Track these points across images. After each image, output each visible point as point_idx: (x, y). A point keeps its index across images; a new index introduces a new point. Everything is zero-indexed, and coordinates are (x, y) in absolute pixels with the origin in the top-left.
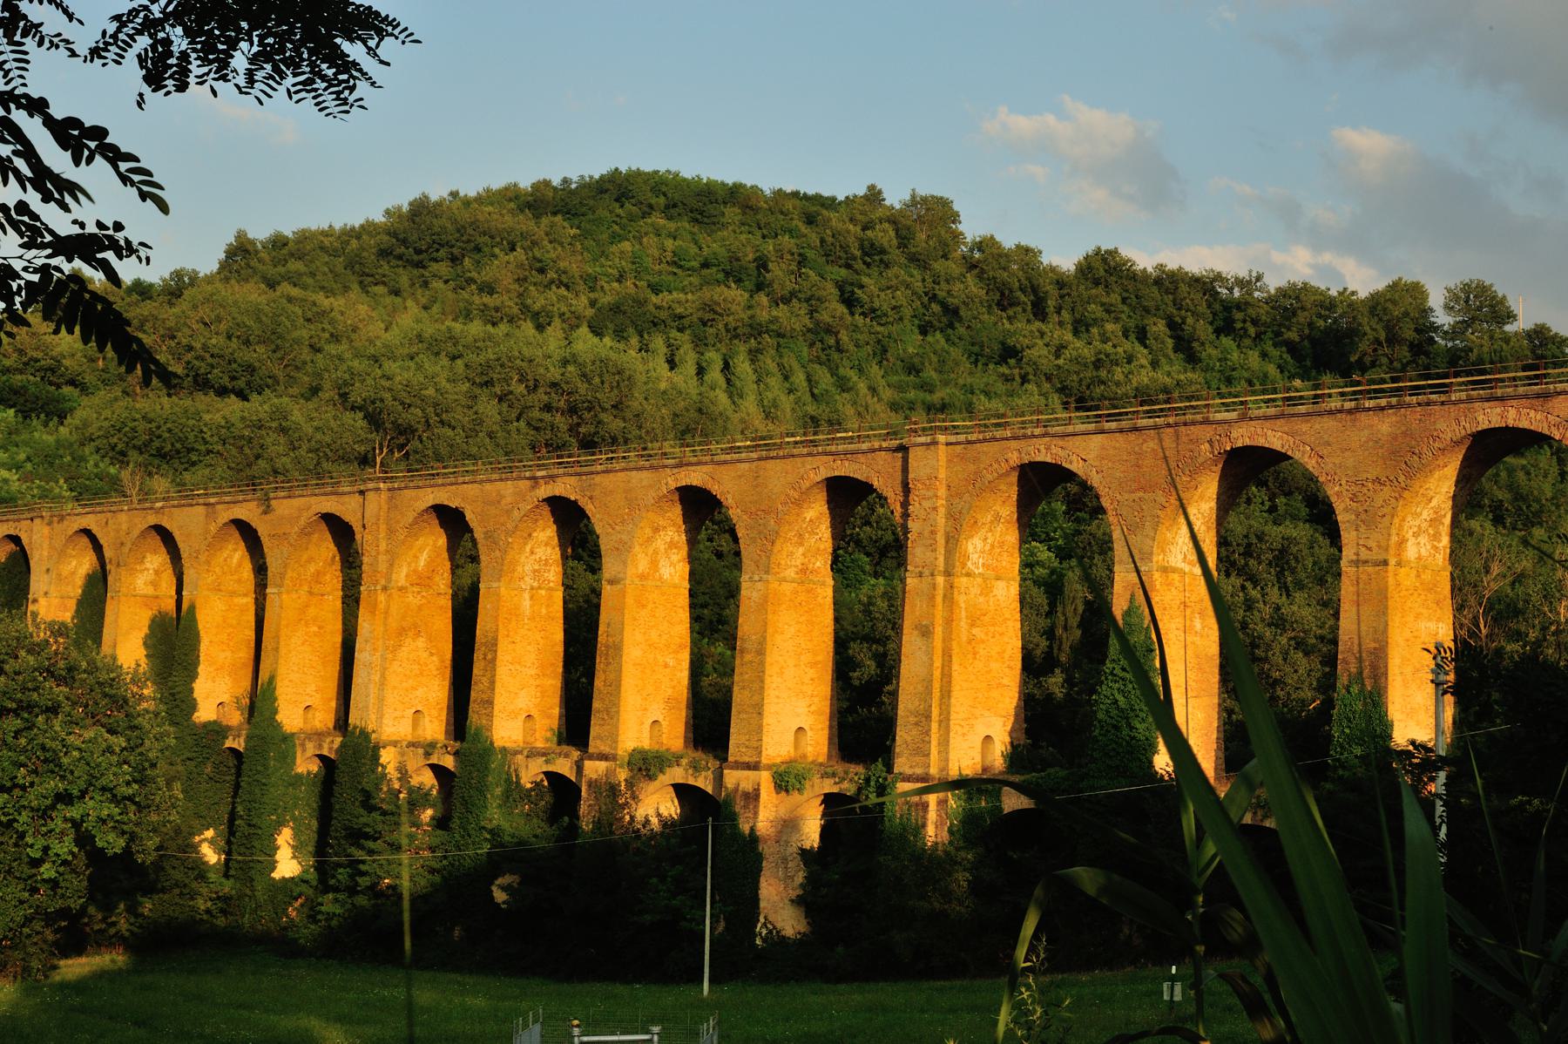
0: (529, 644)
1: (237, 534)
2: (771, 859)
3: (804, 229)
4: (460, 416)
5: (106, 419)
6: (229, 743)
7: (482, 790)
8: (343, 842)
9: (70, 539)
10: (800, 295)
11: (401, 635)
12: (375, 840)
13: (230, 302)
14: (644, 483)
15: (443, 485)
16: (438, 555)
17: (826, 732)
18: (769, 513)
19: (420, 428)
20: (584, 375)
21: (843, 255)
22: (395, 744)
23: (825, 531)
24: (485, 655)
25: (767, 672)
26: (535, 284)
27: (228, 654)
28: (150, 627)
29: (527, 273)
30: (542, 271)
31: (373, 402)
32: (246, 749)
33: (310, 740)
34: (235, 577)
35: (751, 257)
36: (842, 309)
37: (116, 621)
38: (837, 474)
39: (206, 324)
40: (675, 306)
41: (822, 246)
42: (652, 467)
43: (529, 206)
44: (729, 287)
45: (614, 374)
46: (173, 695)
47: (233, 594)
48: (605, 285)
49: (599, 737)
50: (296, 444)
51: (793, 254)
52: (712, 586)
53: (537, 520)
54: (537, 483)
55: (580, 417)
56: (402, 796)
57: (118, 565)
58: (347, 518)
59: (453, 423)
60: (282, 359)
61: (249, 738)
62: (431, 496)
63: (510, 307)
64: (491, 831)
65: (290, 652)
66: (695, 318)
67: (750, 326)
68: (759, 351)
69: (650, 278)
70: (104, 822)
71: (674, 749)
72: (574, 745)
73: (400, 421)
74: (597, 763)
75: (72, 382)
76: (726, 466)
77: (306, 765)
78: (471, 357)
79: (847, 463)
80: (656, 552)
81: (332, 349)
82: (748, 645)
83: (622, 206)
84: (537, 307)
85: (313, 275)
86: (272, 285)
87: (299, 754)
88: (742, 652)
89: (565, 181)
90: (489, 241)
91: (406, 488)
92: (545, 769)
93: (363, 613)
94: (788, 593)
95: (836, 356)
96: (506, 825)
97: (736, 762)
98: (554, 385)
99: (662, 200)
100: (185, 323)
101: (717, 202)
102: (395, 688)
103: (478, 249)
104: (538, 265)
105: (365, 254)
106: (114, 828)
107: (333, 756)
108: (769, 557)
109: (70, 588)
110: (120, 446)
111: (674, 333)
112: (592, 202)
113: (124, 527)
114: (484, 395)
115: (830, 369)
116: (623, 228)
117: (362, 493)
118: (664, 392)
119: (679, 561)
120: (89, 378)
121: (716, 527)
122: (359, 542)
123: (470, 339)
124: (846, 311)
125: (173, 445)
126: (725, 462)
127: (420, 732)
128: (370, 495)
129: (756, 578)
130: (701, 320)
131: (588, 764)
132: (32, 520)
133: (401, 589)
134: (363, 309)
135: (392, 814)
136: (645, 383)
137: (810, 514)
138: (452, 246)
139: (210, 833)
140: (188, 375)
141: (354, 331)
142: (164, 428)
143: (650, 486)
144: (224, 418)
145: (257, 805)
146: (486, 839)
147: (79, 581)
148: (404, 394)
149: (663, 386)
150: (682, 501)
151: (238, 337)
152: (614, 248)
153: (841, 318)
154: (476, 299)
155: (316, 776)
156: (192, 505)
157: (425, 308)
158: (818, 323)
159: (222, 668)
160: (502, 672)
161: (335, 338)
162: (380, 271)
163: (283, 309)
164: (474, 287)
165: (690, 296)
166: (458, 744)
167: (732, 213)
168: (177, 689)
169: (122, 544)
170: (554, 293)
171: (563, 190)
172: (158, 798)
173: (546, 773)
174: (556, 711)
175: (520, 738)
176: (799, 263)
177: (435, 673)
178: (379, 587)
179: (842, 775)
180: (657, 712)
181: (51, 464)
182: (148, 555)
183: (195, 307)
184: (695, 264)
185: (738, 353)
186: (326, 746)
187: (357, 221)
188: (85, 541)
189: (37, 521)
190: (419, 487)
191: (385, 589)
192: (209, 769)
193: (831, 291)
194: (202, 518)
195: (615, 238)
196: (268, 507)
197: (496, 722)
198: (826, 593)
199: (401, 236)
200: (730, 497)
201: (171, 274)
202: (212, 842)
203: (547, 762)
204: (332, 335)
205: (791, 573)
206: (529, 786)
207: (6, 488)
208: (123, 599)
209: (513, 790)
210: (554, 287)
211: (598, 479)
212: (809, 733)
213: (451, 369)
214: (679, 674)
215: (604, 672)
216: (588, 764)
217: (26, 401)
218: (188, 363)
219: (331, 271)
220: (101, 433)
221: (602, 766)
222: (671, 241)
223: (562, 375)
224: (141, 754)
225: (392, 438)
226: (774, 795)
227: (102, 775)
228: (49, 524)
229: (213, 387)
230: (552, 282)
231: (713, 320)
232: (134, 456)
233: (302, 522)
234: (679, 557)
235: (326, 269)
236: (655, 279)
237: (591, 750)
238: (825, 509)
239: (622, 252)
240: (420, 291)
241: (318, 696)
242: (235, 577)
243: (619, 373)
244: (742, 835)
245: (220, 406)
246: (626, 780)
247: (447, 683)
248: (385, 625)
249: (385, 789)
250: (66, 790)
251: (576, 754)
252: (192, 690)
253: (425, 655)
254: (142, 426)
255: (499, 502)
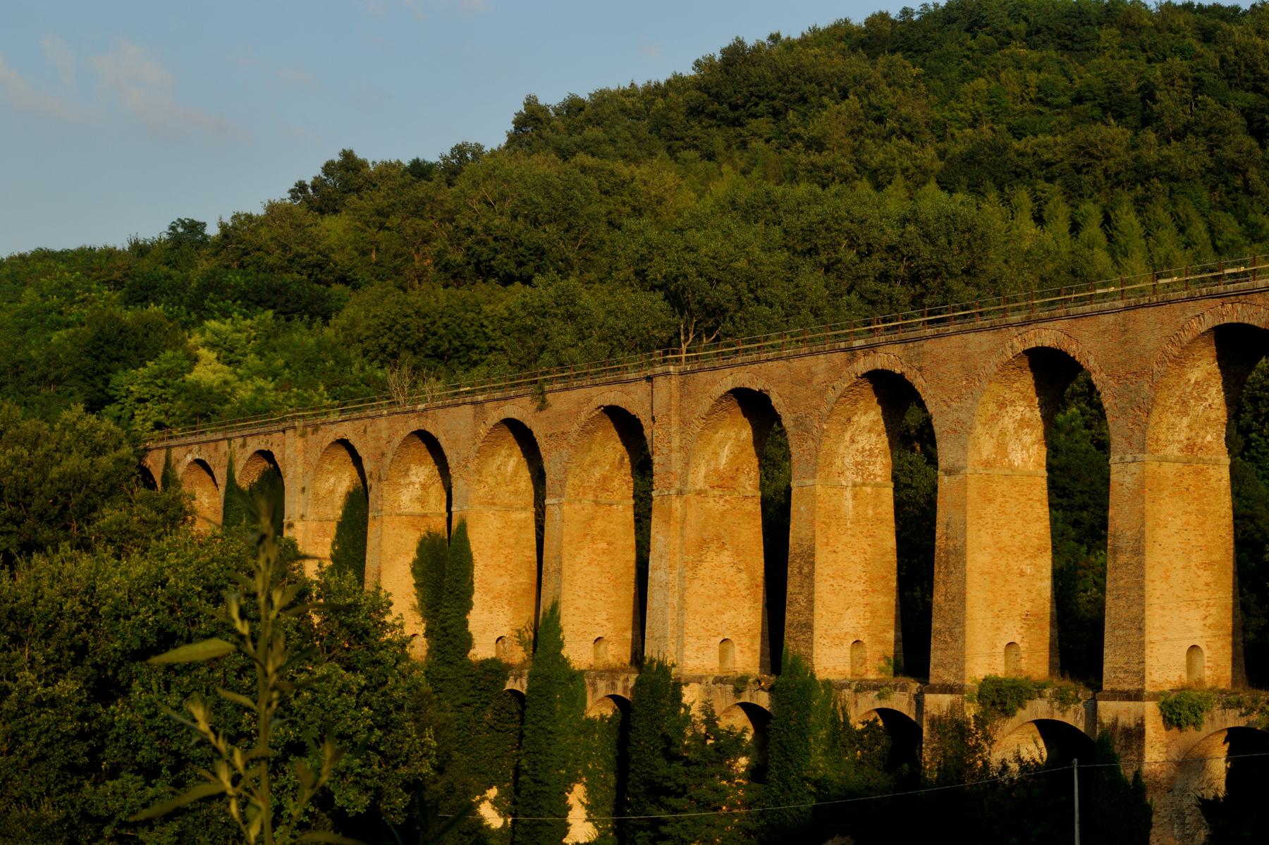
0: (854, 553)
1: (511, 437)
2: (1163, 813)
3: (1199, 47)
4: (781, 291)
5: (375, 316)
6: (510, 685)
7: (803, 733)
8: (642, 800)
9: (327, 452)
10: (1196, 128)
11: (701, 548)
12: (679, 796)
13: (514, 176)
14: (985, 348)
15: (743, 364)
16: (743, 450)
17: (1229, 650)
18: (1142, 376)
19: (732, 307)
20: (927, 235)
21: (1248, 75)
22: (699, 680)
23: (1216, 396)
24: (801, 568)
25: (1147, 577)
26: (872, 136)
27: (507, 579)
28: (419, 551)
29: (862, 124)
30: (880, 120)
31: (676, 280)
32: (528, 691)
33: (601, 678)
34: (512, 488)
35: (1134, 86)
36: (1250, 142)
37: (380, 545)
38: (1227, 320)
39: (488, 204)
40: (1040, 151)
41: (1222, 67)
42: (993, 328)
43: (863, 44)
44: (1107, 125)
45: (963, 232)
46: (444, 629)
47: (509, 508)
48: (956, 132)
49: (942, 665)
50: (587, 333)
51: (1186, 79)
52: (1092, 483)
53: (856, 401)
54: (854, 355)
55: (924, 286)
56: (709, 742)
57: (380, 480)
58: (634, 410)
59: (770, 299)
60: (576, 239)
61: (532, 678)
62: (730, 378)
63: (843, 165)
64: (816, 783)
65: (574, 573)
66: (1066, 164)
67: (1135, 169)
68: (1146, 199)
69: (1010, 120)
70: (343, 775)
71: (1035, 676)
72: (912, 676)
73: (707, 300)
74: (940, 696)
75: (343, 280)
76: (1086, 321)
77: (598, 708)
78: (788, 220)
79: (1239, 307)
80: (1003, 433)
81: (631, 223)
82: (1122, 544)
83: (974, 37)
84: (874, 163)
85: (613, 142)
86: (565, 155)
87: (589, 696)
88: (1115, 552)
89: (906, 12)
90: (817, 89)
91: (700, 370)
92: (878, 706)
93: (654, 522)
94: (1170, 476)
95: (1244, 200)
96: (832, 775)
97: (1113, 691)
98: (891, 249)
99: (1023, 26)
100: (466, 205)
101: (1090, 23)
102: (696, 612)
103: (802, 99)
104: (876, 113)
105: (672, 114)
106: (356, 783)
107: (628, 697)
108: (1143, 432)
109: (328, 510)
110: (390, 348)
111: (1041, 184)
112: (937, 35)
113: (384, 434)
114: (806, 266)
115: (1237, 216)
116: (976, 62)
117: (649, 379)
118: (1029, 252)
119: (1033, 444)
120: (362, 274)
121: (1095, 411)
122: (648, 439)
123: (793, 203)
124: (1255, 143)
125: (450, 342)
126: (1084, 315)
127: (729, 665)
128: (659, 382)
129: (1129, 458)
130: (1074, 165)
131: (929, 698)
132: (284, 431)
133: (699, 493)
134: (670, 178)
135: (697, 764)
136: (1005, 243)
137: (1195, 375)
138: (773, 98)
139: (493, 793)
140: (469, 263)
141: (659, 202)
142: (439, 324)
143: (992, 351)
144: (507, 308)
145: (542, 758)
146: (810, 793)
147: (339, 500)
148: (712, 269)
149: (1026, 245)
150: (1034, 367)
151: (526, 216)
152: (966, 88)
153: (1250, 153)
154: (803, 159)
155: (611, 721)
156: (458, 405)
157: (744, 173)
158: (1220, 162)
159: (500, 596)
160: (822, 588)
161: (638, 212)
162: (690, 132)
163: (576, 180)
164: (799, 144)
165: (1059, 138)
166: (773, 678)
167: (1109, 35)
168: (449, 622)
169: (383, 454)
170: (892, 147)
171: (904, 22)
172: (406, 746)
173: (879, 711)
174: (891, 635)
175: (848, 669)
176: (1195, 89)
177: (744, 593)
178: (673, 492)
179: (1249, 703)
180: (1013, 631)
181: (312, 370)
182: (413, 466)
183: (476, 185)
184: (1065, 100)
185: (1121, 203)
186: (620, 685)
187: (662, 77)
188: (343, 453)
189: (290, 433)
190: (715, 369)
191: (680, 493)
192: (489, 716)
193: (1235, 120)
194: (470, 420)
195: (967, 75)
196: (544, 401)
197: (816, 650)
198: (1221, 475)
199: (713, 91)
200: (1091, 358)
201: (453, 150)
202: (495, 803)
203: (880, 697)
204: (634, 209)
205: (1173, 451)
206: (860, 727)
207: (260, 398)
208: (386, 519)
209: (841, 733)
210: (894, 138)
211: (927, 345)
212: (1206, 653)
213: (766, 235)
214: (1039, 584)
215: (945, 583)
216: (929, 698)
217: (287, 301)
218: (468, 249)
219: (634, 137)
220: (369, 333)
221: (945, 700)
222: (1035, 74)
223: (901, 236)
224: (384, 694)
225: (699, 321)
226: (1163, 731)
227: (339, 719)
228: (303, 435)
229: (497, 275)
230: (893, 132)
231: (1089, 165)
232: (407, 356)
233: (583, 418)
234: (1034, 438)
235: (629, 135)
236: (1016, 122)
237: (932, 680)
238: (1214, 367)
239: (975, 92)
240: (737, 154)
241: (610, 625)
242: (512, 488)
243: (969, 230)
244: (1125, 783)
245: (502, 295)
246: (975, 716)
247: (760, 606)
248: (682, 536)
249: (689, 733)
250: (298, 738)
251: (914, 686)
252: (466, 623)
253: (732, 571)
254: (414, 322)
255: (810, 381)
